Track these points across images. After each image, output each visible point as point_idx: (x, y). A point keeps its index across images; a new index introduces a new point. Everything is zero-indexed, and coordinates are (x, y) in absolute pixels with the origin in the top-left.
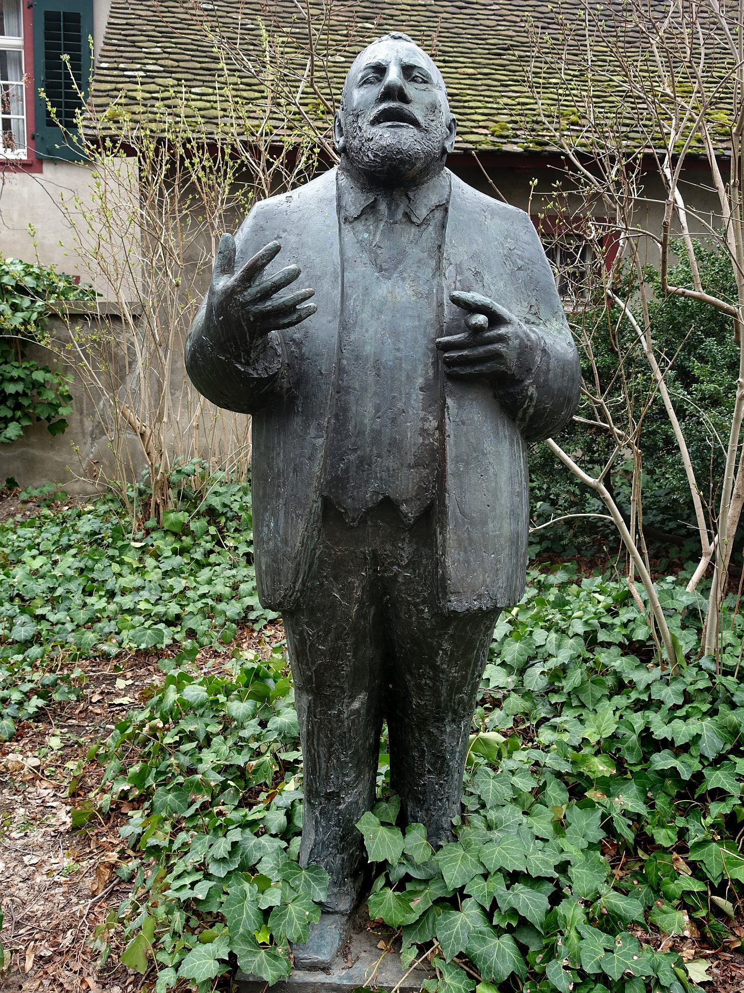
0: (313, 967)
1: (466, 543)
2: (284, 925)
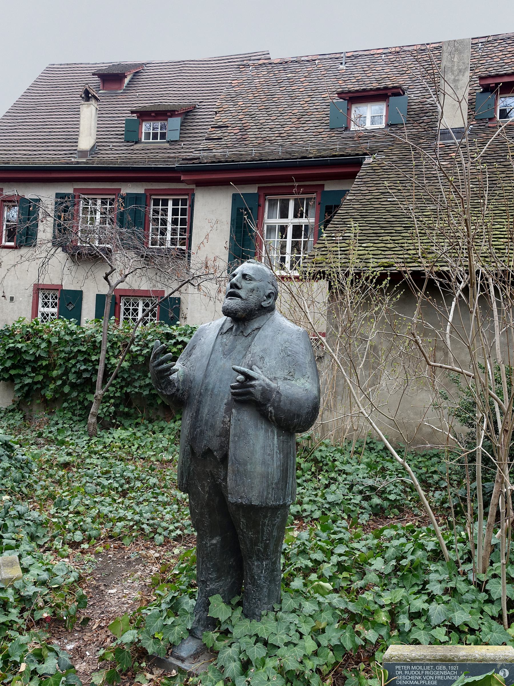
0: (179, 658)
1: (236, 472)
2: (170, 634)
